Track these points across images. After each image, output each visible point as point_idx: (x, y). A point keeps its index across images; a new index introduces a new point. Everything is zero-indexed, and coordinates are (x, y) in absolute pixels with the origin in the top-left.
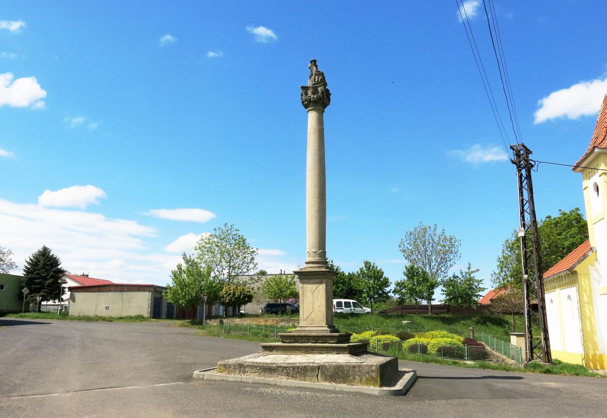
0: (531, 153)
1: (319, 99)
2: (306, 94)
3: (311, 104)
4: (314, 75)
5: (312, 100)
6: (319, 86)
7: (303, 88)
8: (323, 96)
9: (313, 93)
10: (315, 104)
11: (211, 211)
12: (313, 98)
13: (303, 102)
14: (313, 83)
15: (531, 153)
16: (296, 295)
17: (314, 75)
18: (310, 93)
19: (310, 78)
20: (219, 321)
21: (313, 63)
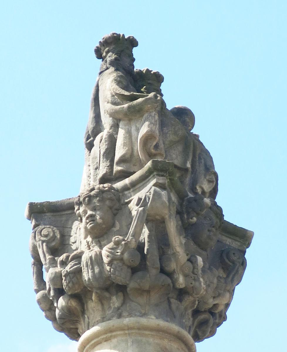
0: (133, 43)
1: (137, 262)
2: (58, 247)
3: (93, 304)
4: (107, 121)
5: (87, 275)
6: (135, 186)
7: (38, 212)
8: (161, 239)
9: (99, 234)
10: (116, 301)
11: (191, 166)
12: (97, 260)
13: (48, 306)
14: (103, 171)
15: (133, 43)
16: (224, 309)
17: (107, 121)
18: (79, 236)
19: (90, 146)
20: (182, 262)
21: (111, 57)
